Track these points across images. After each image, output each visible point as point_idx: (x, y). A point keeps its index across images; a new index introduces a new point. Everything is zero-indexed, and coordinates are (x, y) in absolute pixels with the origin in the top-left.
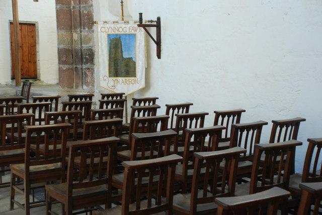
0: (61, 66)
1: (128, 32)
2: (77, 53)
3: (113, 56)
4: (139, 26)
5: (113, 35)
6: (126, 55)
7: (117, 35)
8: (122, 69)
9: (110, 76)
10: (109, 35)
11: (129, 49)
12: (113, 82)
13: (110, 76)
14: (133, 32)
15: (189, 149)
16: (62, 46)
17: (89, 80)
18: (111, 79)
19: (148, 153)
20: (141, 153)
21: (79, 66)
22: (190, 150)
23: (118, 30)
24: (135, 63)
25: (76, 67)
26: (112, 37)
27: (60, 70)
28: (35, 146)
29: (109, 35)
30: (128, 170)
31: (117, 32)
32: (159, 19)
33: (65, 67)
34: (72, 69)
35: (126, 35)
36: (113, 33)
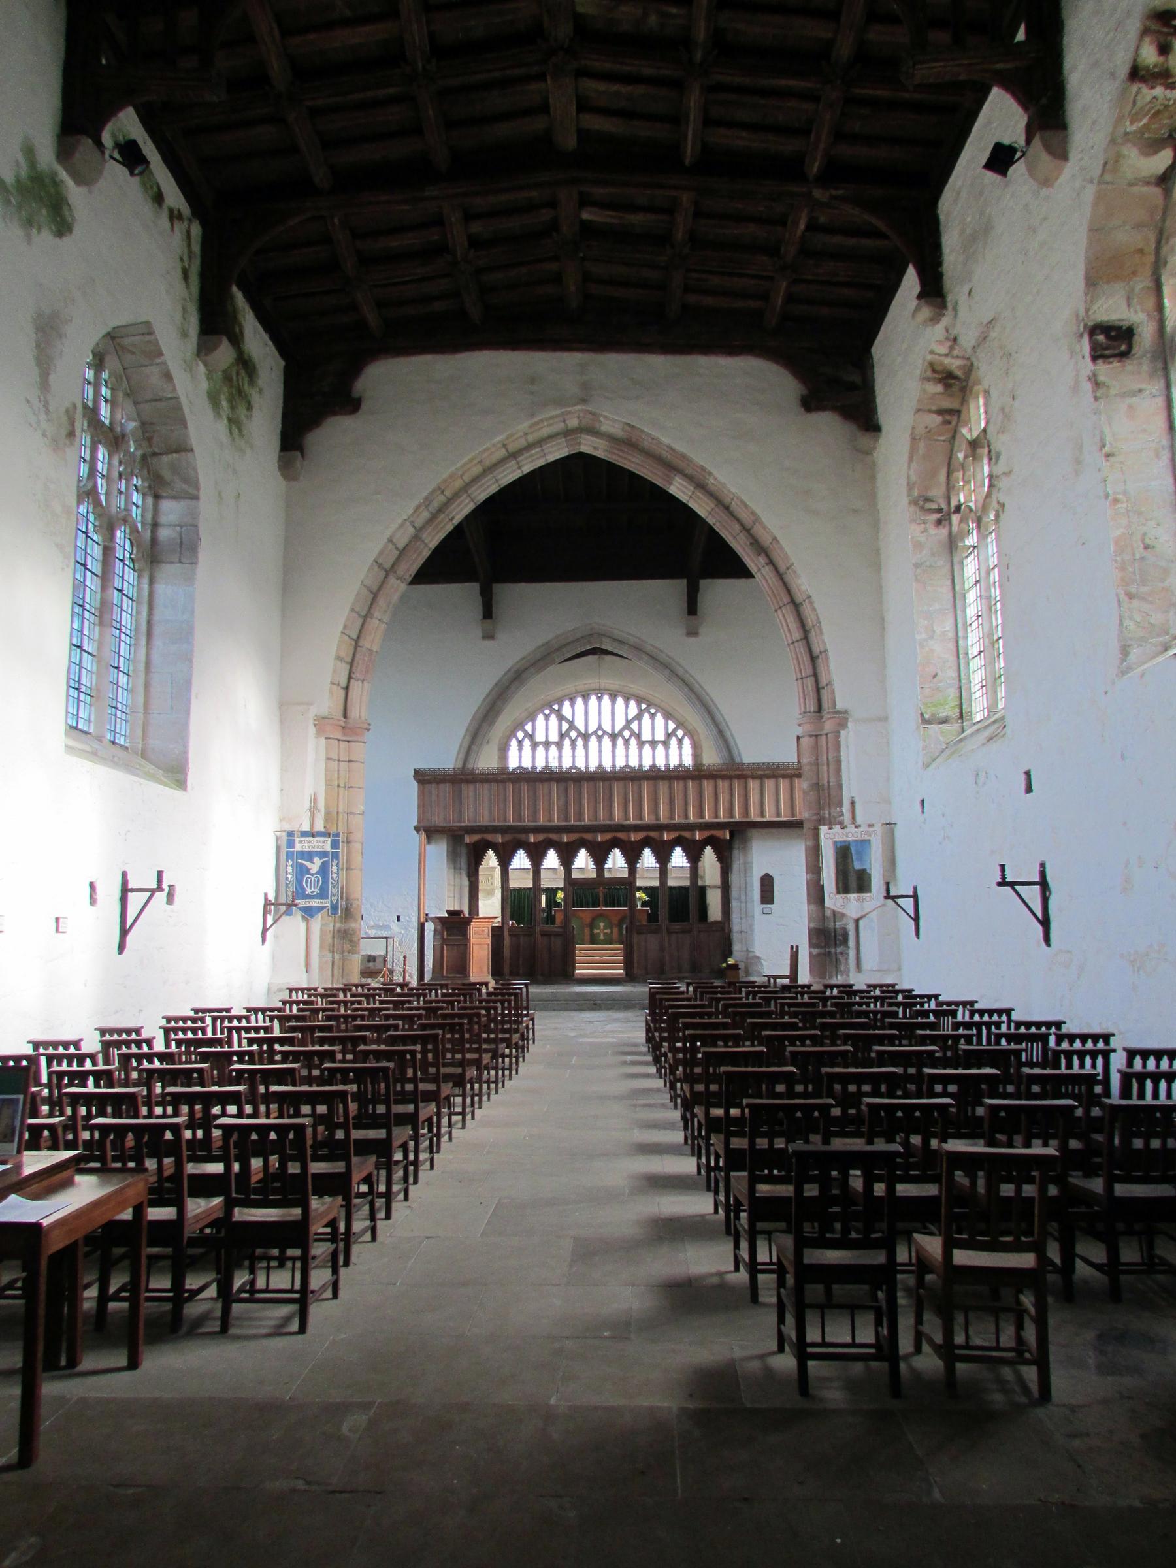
0: (813, 950)
1: (859, 838)
2: (829, 932)
3: (841, 867)
4: (886, 898)
5: (841, 842)
6: (857, 866)
7: (845, 842)
8: (853, 883)
9: (838, 892)
10: (835, 843)
11: (860, 859)
12: (841, 900)
13: (838, 892)
14: (866, 837)
15: (175, 1161)
16: (812, 925)
17: (843, 967)
18: (839, 896)
19: (904, 1042)
20: (1093, 1114)
21: (833, 950)
22: (172, 1159)
23: (847, 836)
24: (869, 876)
25: (830, 952)
26: (839, 845)
27: (810, 953)
28: (766, 1141)
29: (835, 843)
30: (1153, 88)
31: (845, 838)
32: (915, 889)
33: (815, 951)
34: (824, 954)
35: (856, 841)
36: (840, 839)
